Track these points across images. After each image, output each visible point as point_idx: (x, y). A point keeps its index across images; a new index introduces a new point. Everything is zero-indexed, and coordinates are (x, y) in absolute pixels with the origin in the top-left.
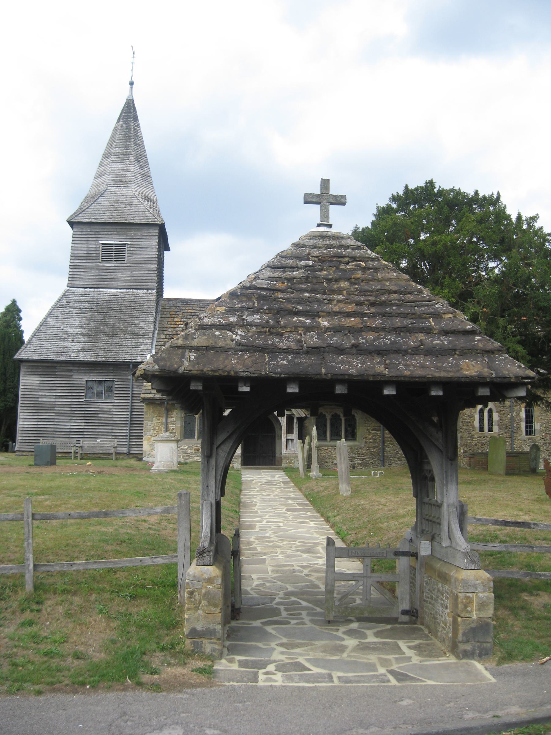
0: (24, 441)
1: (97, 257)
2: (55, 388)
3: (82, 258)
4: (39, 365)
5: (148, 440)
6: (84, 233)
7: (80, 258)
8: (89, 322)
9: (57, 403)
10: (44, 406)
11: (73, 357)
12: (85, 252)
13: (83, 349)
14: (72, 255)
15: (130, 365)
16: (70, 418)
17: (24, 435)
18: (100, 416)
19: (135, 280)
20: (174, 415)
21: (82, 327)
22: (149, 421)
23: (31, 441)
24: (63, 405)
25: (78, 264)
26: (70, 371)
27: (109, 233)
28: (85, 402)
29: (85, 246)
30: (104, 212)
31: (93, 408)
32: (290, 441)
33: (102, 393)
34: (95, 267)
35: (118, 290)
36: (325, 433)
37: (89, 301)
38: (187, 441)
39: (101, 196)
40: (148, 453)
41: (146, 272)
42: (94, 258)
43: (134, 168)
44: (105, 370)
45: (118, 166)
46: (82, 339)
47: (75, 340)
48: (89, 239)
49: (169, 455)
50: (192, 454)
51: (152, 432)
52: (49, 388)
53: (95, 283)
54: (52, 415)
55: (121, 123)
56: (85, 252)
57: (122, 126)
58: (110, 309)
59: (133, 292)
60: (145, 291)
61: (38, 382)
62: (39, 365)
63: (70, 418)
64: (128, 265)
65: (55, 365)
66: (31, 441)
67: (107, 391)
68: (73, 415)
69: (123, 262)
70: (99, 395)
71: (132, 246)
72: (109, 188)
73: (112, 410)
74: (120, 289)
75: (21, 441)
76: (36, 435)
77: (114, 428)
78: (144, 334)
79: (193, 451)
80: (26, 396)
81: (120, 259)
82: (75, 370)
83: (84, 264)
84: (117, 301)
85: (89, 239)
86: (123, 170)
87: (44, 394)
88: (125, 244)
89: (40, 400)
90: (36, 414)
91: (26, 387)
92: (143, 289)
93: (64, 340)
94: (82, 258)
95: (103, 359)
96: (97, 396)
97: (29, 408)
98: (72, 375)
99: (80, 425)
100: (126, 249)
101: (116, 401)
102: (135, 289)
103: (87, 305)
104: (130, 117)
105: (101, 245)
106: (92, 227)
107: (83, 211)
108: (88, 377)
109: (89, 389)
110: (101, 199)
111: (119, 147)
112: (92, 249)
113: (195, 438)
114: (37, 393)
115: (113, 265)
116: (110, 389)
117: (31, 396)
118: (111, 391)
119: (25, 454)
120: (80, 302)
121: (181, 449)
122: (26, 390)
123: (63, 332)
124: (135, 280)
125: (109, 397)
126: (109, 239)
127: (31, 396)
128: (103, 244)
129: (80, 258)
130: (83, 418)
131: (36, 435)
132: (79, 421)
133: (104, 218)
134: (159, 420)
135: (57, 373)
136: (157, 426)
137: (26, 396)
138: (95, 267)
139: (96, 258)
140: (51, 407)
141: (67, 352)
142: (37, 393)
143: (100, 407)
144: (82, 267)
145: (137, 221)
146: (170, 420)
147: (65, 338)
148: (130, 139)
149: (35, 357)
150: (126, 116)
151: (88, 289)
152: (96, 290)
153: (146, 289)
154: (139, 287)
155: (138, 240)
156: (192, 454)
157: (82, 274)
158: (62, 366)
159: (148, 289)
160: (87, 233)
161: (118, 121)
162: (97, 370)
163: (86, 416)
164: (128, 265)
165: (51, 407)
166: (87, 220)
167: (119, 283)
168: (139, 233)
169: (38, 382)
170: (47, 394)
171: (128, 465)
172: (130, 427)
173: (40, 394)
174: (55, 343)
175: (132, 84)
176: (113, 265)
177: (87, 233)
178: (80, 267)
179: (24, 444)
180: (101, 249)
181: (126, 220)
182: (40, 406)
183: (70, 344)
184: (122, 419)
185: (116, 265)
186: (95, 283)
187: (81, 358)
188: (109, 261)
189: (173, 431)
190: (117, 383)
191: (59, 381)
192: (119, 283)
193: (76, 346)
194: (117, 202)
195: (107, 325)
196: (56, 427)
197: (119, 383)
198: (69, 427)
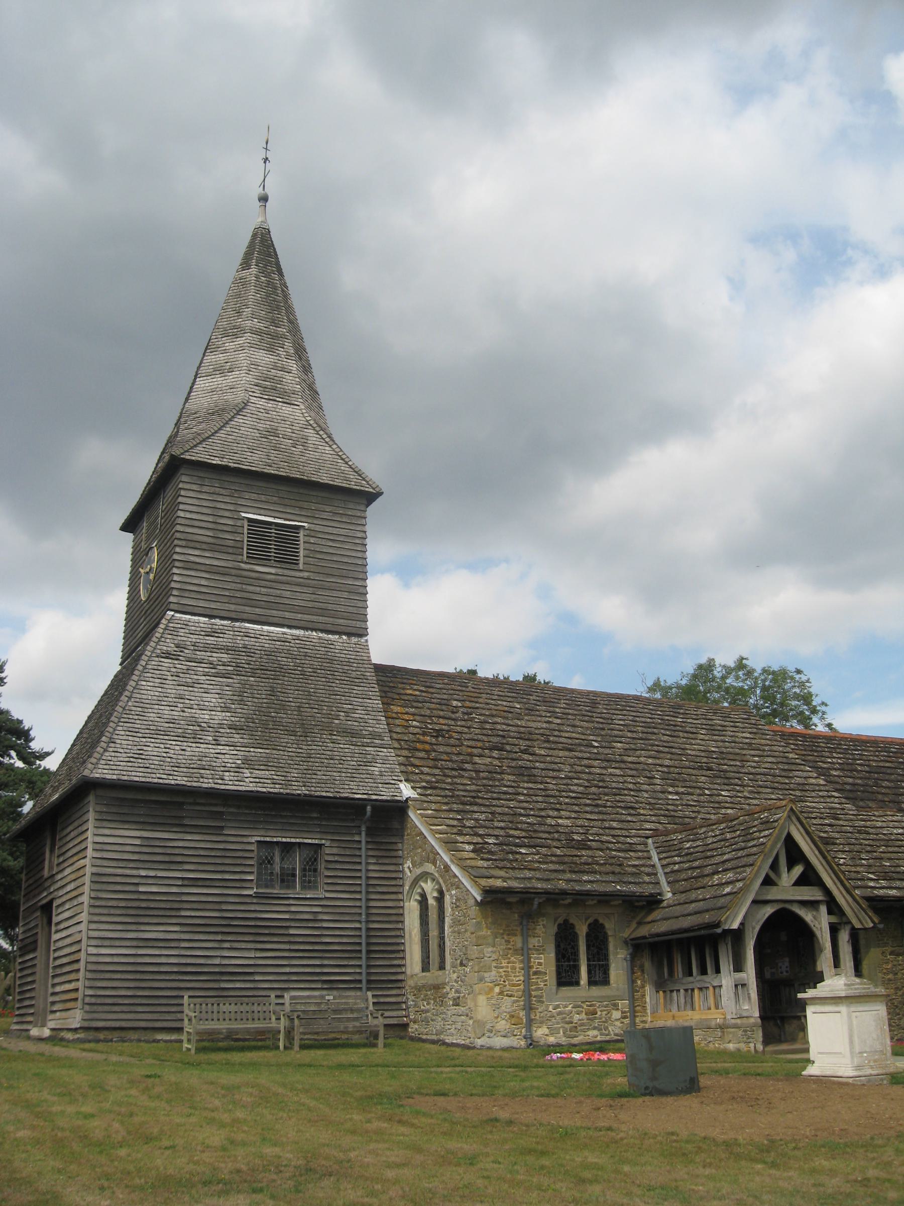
0: (99, 1001)
1: (237, 549)
2: (179, 859)
3: (204, 546)
4: (139, 797)
5: (487, 994)
6: (205, 489)
7: (198, 545)
8: (240, 696)
9: (185, 898)
10: (152, 905)
11: (229, 783)
12: (210, 533)
13: (248, 763)
14: (363, 521)
15: (365, 807)
16: (219, 937)
17: (100, 984)
18: (292, 932)
19: (323, 612)
20: (540, 929)
21: (226, 709)
22: (488, 944)
23: (120, 1001)
24: (202, 905)
25: (192, 559)
26: (219, 815)
27: (263, 498)
28: (258, 896)
29: (210, 519)
30: (252, 450)
31: (274, 913)
32: (740, 987)
33: (294, 875)
34: (234, 572)
35: (285, 630)
36: (576, 969)
37: (227, 649)
38: (566, 991)
39: (237, 414)
40: (488, 1027)
41: (345, 595)
42: (231, 551)
43: (293, 366)
44: (303, 818)
45: (264, 358)
46: (237, 738)
47: (223, 740)
48: (219, 505)
49: (875, 1036)
50: (582, 1025)
51: (494, 973)
52: (167, 859)
53: (233, 607)
54: (172, 931)
55: (254, 270)
56: (210, 533)
57: (257, 277)
58: (281, 670)
59: (320, 638)
60: (344, 637)
61: (138, 842)
62: (139, 797)
63: (219, 937)
64: (306, 574)
65: (180, 799)
66: (120, 1001)
67: (304, 870)
68: (229, 928)
69: (295, 567)
70: (287, 879)
71: (311, 533)
72: (253, 400)
73: (321, 917)
74: (290, 627)
75: (93, 1000)
76: (132, 984)
77: (326, 962)
78: (374, 735)
79: (583, 1016)
80: (105, 879)
81: (287, 558)
82: (232, 813)
83: (208, 562)
84: (289, 654)
85: (219, 505)
86: (275, 368)
87: (152, 873)
88: (298, 528)
89: (142, 889)
90: (134, 927)
91: (106, 855)
92: (340, 633)
93: (195, 738)
94: (204, 546)
95: (304, 791)
96: (282, 881)
97: (112, 911)
98: (222, 828)
99: (241, 956)
100: (302, 538)
101: (328, 895)
102: (322, 631)
103: (225, 657)
104: (270, 262)
105: (246, 523)
106: (224, 478)
107: (204, 440)
108: (262, 833)
109: (265, 862)
110: (239, 420)
111: (260, 319)
112: (225, 528)
113: (577, 983)
114: (134, 872)
115: (273, 571)
116: (311, 867)
117: (118, 879)
118: (315, 870)
119: (101, 1036)
120: (207, 648)
121: (560, 1013)
122: (105, 863)
123: (185, 718)
124: (323, 612)
125: (308, 885)
126: (262, 512)
127: (118, 879)
128: (250, 520)
129: (198, 545)
130: (251, 938)
131: (132, 984)
132: (243, 945)
133: (255, 461)
134: (508, 942)
135: (187, 822)
136: (505, 956)
137: (105, 879)
138: (234, 572)
139: (234, 550)
140: (169, 909)
141: (211, 768)
142: (134, 872)
143: (293, 909)
144: (203, 568)
145: (325, 479)
146: (534, 942)
147: (195, 733)
148: (278, 308)
149: (137, 776)
150: (262, 260)
151: (217, 621)
152: (237, 624)
153: (345, 634)
154: (329, 627)
155: (325, 523)
156: (582, 1025)
157: (203, 582)
158: (198, 804)
159: (349, 635)
160: (212, 490)
161: (246, 264)
162: (282, 817)
163: (259, 931)
164: (306, 574)
165: (169, 909)
166: (216, 461)
167: (287, 615)
168: (328, 509)
169: (138, 842)
170: (160, 874)
171: (759, 1071)
172: (368, 958)
173: (143, 873)
174: (175, 747)
175: (264, 199)
176: (273, 571)
177: (212, 490)
178: (199, 567)
179: (100, 1008)
180: (246, 531)
181: (303, 473)
182: (144, 905)
183: (212, 750)
184: (345, 940)
185: (280, 571)
186: (233, 607)
187: (248, 783)
188: (265, 560)
189: (541, 969)
190: (330, 850)
191: (192, 839)
192: (287, 615)
193: (230, 757)
194: (274, 432)
195: (283, 707)
196: (183, 961)
197: (335, 851)
198: (217, 961)
